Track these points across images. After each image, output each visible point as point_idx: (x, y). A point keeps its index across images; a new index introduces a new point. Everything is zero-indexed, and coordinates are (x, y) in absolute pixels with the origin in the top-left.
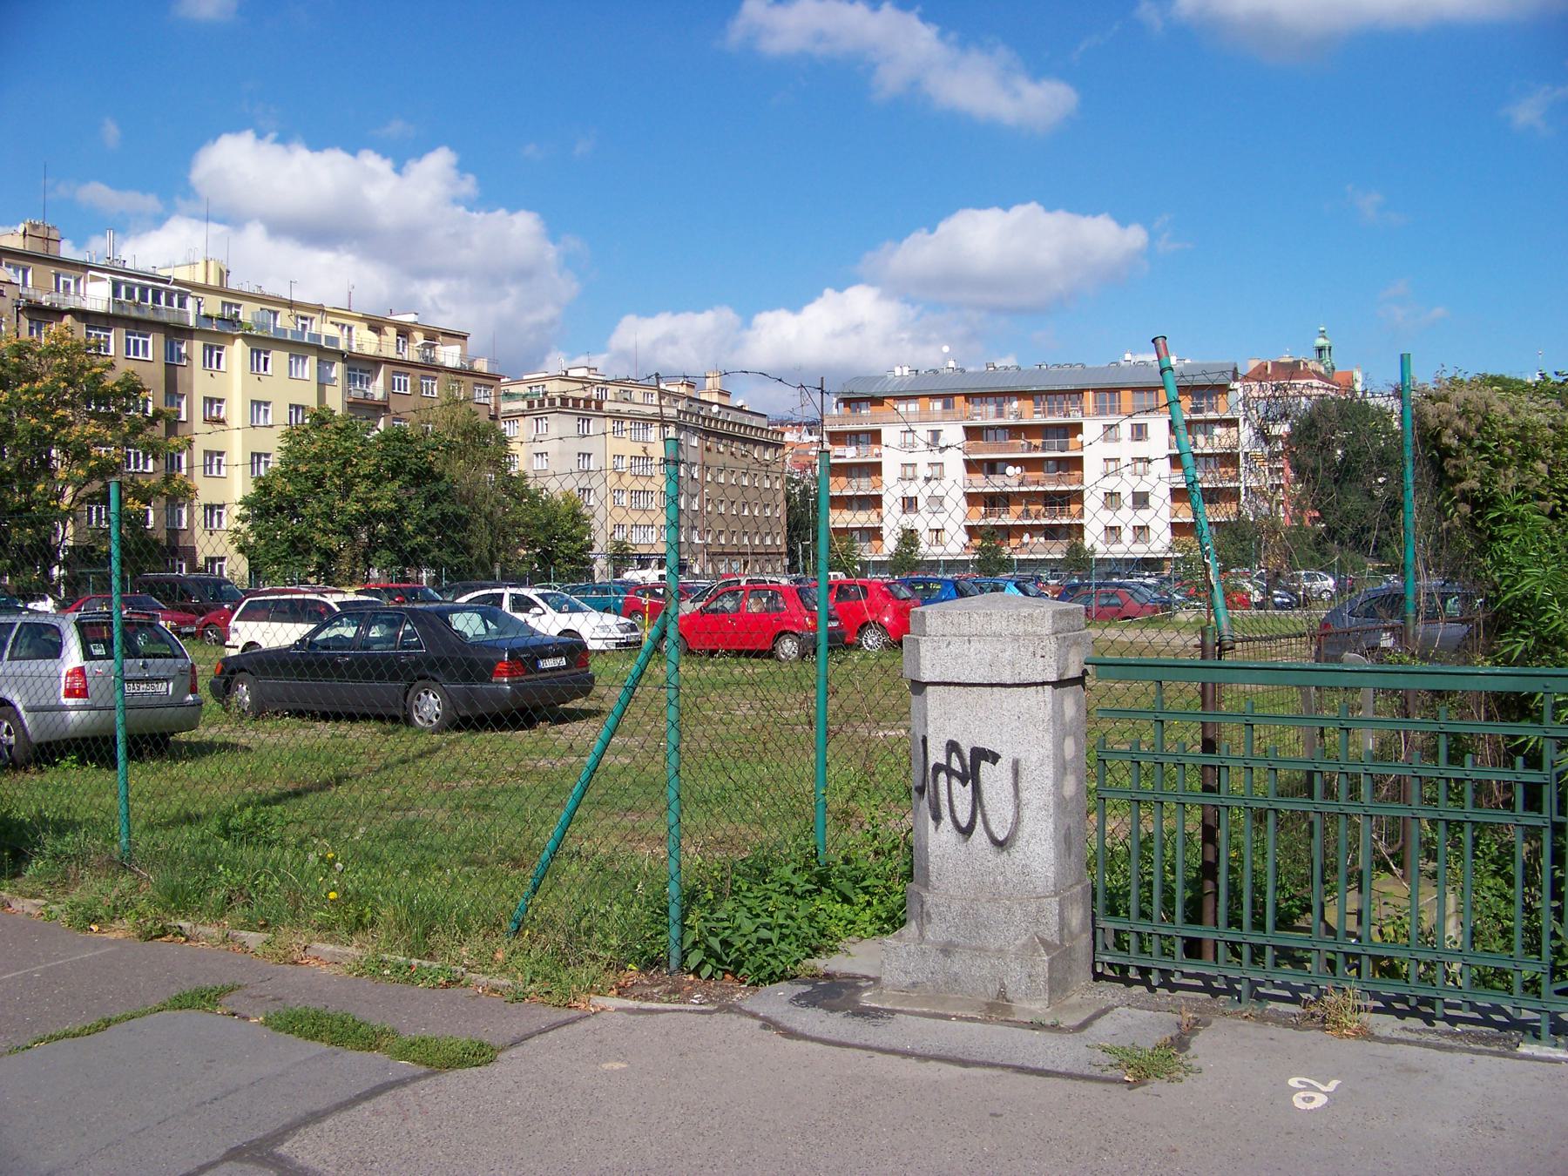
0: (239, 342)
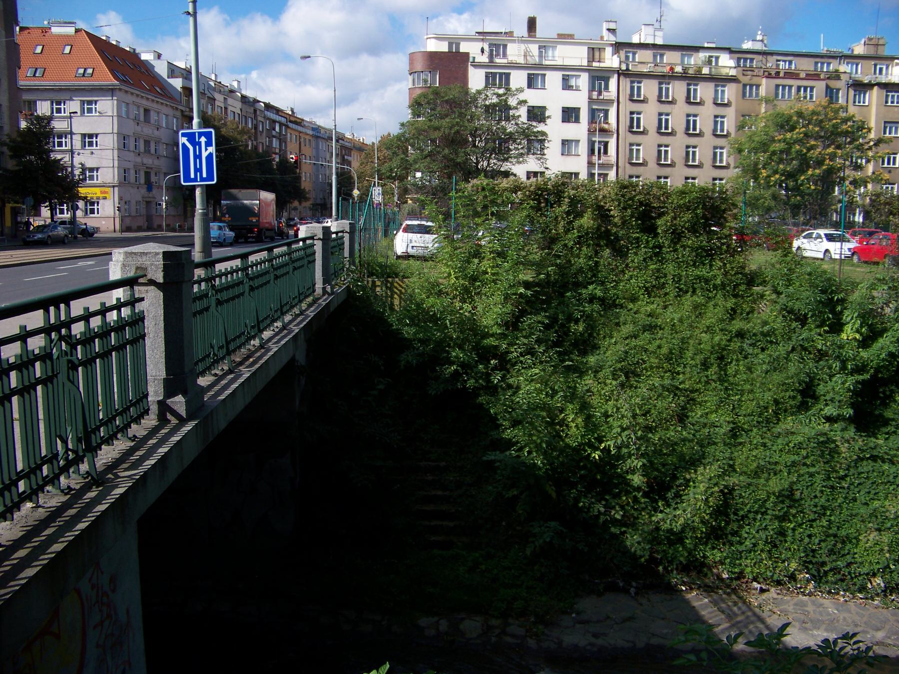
0: (876, 88)
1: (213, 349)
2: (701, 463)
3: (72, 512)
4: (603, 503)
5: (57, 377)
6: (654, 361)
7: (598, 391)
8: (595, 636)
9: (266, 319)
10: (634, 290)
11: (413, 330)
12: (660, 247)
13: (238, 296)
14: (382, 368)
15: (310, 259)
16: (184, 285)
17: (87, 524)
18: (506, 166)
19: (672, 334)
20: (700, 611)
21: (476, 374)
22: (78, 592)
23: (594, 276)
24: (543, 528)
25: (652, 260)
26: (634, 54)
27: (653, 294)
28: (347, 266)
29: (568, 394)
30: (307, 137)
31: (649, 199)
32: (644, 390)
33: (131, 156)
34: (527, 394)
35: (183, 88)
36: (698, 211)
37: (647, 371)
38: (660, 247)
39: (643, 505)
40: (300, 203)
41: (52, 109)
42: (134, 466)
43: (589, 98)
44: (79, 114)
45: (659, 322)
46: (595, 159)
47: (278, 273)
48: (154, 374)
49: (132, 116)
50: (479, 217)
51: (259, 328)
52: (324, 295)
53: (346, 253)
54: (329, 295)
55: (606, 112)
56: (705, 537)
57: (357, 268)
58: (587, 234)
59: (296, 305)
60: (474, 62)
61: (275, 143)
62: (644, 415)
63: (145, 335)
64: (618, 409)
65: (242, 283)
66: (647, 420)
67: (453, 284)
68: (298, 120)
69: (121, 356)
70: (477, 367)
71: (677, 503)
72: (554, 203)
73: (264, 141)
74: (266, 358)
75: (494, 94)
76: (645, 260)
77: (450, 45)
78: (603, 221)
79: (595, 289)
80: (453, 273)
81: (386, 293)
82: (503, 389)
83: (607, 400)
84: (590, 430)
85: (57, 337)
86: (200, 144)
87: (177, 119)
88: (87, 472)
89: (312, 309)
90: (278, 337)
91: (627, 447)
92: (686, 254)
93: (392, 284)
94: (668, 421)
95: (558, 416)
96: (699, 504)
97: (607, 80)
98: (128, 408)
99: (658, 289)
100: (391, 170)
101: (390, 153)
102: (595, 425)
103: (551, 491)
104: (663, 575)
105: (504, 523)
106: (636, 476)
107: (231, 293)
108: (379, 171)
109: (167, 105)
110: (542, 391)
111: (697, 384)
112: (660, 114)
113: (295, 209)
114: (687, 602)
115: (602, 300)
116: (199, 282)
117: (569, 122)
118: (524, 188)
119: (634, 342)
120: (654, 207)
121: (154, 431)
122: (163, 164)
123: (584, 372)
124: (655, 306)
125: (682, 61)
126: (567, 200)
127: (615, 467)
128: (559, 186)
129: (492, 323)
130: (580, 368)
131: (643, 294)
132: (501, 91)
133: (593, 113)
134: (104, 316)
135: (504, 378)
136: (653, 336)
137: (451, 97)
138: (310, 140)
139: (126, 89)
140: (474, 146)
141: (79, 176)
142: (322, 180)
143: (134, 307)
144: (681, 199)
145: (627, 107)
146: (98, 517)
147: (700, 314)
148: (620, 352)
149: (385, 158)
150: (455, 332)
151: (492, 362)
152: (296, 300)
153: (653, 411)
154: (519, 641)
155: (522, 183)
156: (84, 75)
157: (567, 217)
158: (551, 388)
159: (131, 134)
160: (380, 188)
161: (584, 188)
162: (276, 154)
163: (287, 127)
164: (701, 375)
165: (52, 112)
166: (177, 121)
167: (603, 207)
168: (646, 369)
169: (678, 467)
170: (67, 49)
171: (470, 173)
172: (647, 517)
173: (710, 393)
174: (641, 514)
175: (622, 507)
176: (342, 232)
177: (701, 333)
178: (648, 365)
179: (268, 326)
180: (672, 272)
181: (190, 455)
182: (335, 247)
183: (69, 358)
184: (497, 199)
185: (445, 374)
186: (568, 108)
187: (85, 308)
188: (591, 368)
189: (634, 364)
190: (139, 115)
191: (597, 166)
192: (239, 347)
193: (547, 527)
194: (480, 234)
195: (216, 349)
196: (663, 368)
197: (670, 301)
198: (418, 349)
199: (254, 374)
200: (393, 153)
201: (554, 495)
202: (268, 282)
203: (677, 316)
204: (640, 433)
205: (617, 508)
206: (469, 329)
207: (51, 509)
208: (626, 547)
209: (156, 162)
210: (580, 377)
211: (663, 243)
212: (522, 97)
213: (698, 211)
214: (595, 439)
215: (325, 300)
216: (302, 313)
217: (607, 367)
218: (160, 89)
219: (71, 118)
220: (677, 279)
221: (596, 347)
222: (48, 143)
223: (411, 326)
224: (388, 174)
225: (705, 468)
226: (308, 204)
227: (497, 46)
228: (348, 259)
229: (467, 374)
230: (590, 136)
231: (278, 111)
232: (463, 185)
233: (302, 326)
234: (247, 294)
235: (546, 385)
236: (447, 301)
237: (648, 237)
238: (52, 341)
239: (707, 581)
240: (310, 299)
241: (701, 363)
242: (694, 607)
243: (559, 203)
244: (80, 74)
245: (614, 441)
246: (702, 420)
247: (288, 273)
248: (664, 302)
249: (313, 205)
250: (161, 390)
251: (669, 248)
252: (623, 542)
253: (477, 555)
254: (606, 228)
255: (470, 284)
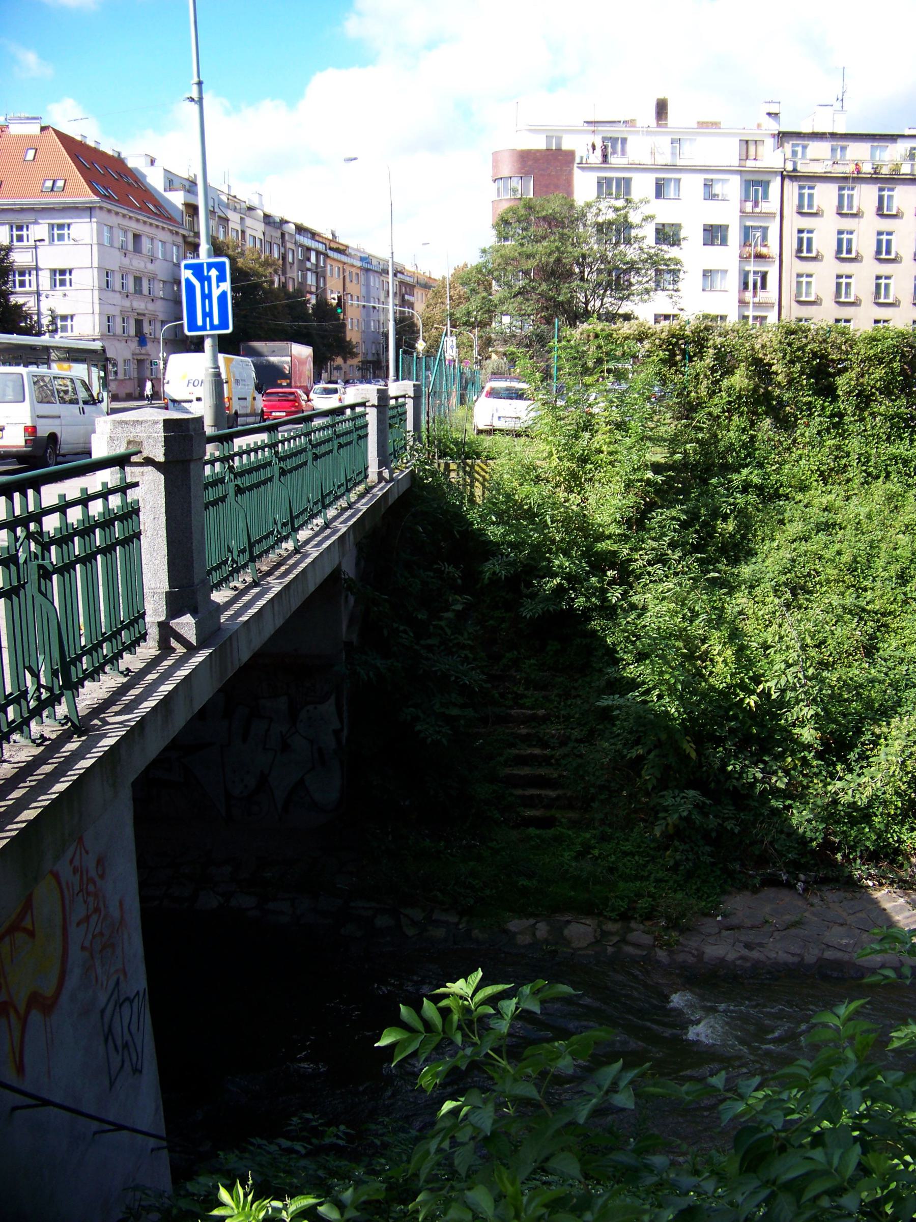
1: (232, 553)
2: (896, 712)
3: (47, 769)
4: (761, 766)
5: (24, 588)
6: (832, 572)
7: (754, 613)
8: (748, 946)
9: (302, 513)
10: (803, 474)
11: (501, 530)
12: (841, 415)
13: (264, 483)
14: (459, 581)
15: (361, 433)
16: (192, 466)
17: (67, 784)
18: (626, 308)
19: (856, 535)
20: (893, 914)
21: (587, 589)
22: (56, 876)
23: (749, 455)
24: (678, 799)
25: (829, 433)
26: (805, 147)
27: (830, 480)
28: (411, 443)
29: (714, 617)
30: (354, 270)
31: (825, 350)
32: (816, 612)
33: (117, 299)
34: (657, 617)
35: (187, 205)
36: (895, 365)
37: (822, 586)
38: (841, 415)
39: (816, 770)
40: (345, 362)
41: (12, 236)
42: (128, 709)
43: (741, 212)
44: (47, 242)
45: (839, 518)
46: (748, 295)
47: (319, 451)
48: (153, 586)
49: (117, 244)
50: (591, 375)
51: (293, 525)
52: (380, 482)
53: (410, 426)
54: (388, 482)
55: (765, 230)
56: (900, 815)
57: (424, 446)
58: (740, 397)
59: (343, 495)
60: (581, 163)
61: (311, 279)
62: (818, 646)
63: (140, 533)
64: (781, 638)
65: (269, 464)
66: (821, 653)
67: (556, 467)
68: (341, 247)
69: (109, 561)
70: (588, 580)
71: (861, 768)
72: (695, 355)
73: (294, 275)
74: (302, 566)
75: (610, 207)
76: (819, 433)
77: (549, 138)
78: (761, 380)
79: (751, 473)
80: (554, 452)
81: (464, 480)
82: (623, 610)
83: (767, 626)
84: (743, 667)
85: (24, 534)
86: (209, 279)
87: (178, 246)
88: (66, 717)
89: (364, 501)
90: (319, 538)
91: (794, 689)
92: (878, 423)
93: (472, 467)
94: (850, 654)
95: (699, 648)
96: (893, 768)
97: (766, 185)
98: (119, 632)
99: (837, 473)
100: (469, 314)
101: (466, 290)
102: (749, 660)
103: (689, 749)
104: (842, 865)
105: (625, 793)
106: (806, 729)
107: (255, 478)
108: (451, 315)
109: (163, 228)
110: (677, 612)
111: (892, 604)
112: (840, 232)
113: (338, 368)
114: (875, 902)
115: (760, 489)
116: (212, 462)
117: (712, 244)
118: (652, 335)
119: (803, 547)
120: (833, 361)
121: (154, 663)
122: (159, 309)
123: (736, 587)
124: (834, 496)
125: (872, 155)
126: (711, 351)
127: (777, 717)
128: (701, 331)
129: (609, 520)
130: (729, 582)
131: (816, 481)
132: (620, 203)
133: (746, 232)
134: (86, 506)
135: (625, 595)
136: (830, 538)
137: (550, 211)
138: (357, 274)
139: (110, 207)
140: (582, 279)
141: (48, 326)
142: (375, 327)
143: (125, 494)
144: (871, 348)
145: (793, 222)
146: (81, 775)
147: (896, 507)
148: (785, 561)
149: (460, 298)
150: (559, 532)
151: (609, 573)
152: (343, 489)
153: (829, 641)
154: (645, 953)
155: (649, 328)
156: (52, 190)
157: (712, 374)
158: (689, 609)
159: (117, 268)
160: (454, 338)
161: (735, 334)
162: (311, 293)
163: (326, 256)
164: (896, 592)
165: (12, 241)
166: (178, 251)
167: (761, 360)
168: (820, 583)
169: (865, 718)
170: (30, 154)
171: (575, 316)
172: (821, 785)
173: (910, 616)
174: (812, 782)
175: (787, 772)
176: (404, 396)
177: (898, 534)
178: (823, 577)
179: (305, 523)
180: (857, 450)
181: (203, 695)
182: (394, 417)
183: (40, 562)
184: (615, 350)
185: (545, 590)
186: (711, 226)
187: (60, 496)
188: (745, 582)
189: (804, 576)
190: (126, 242)
191: (751, 305)
192: (267, 552)
193: (683, 797)
194: (592, 398)
195: (235, 553)
196: (844, 582)
197: (854, 489)
198: (507, 556)
199: (287, 588)
200: (471, 290)
201: (693, 755)
202: (305, 463)
203: (863, 511)
204: (811, 671)
205: (780, 774)
206: (578, 529)
207: (20, 765)
208: (791, 826)
209: (151, 306)
210: (730, 594)
211: (845, 409)
212: (647, 210)
213: (895, 365)
214: (750, 678)
215: (381, 490)
216: (350, 506)
217: (766, 580)
218: (155, 206)
219: (36, 247)
220: (863, 459)
221: (751, 553)
222: (6, 283)
223: (498, 524)
224: (465, 319)
225: (901, 720)
226: (355, 362)
227: (614, 140)
228: (412, 433)
229: (575, 590)
230: (743, 264)
231: (313, 235)
232: (567, 331)
233: (351, 523)
234: (276, 479)
235: (683, 604)
236: (546, 489)
237: (824, 401)
238: (17, 539)
239: (902, 873)
240: (361, 488)
241: (897, 575)
242: (885, 910)
243: (701, 355)
244: (47, 188)
245: (775, 681)
246: (897, 653)
247: (331, 451)
248: (845, 491)
249: (363, 362)
250: (163, 608)
251: (853, 416)
252: (788, 819)
253: (588, 835)
254: (766, 389)
255: (578, 466)
